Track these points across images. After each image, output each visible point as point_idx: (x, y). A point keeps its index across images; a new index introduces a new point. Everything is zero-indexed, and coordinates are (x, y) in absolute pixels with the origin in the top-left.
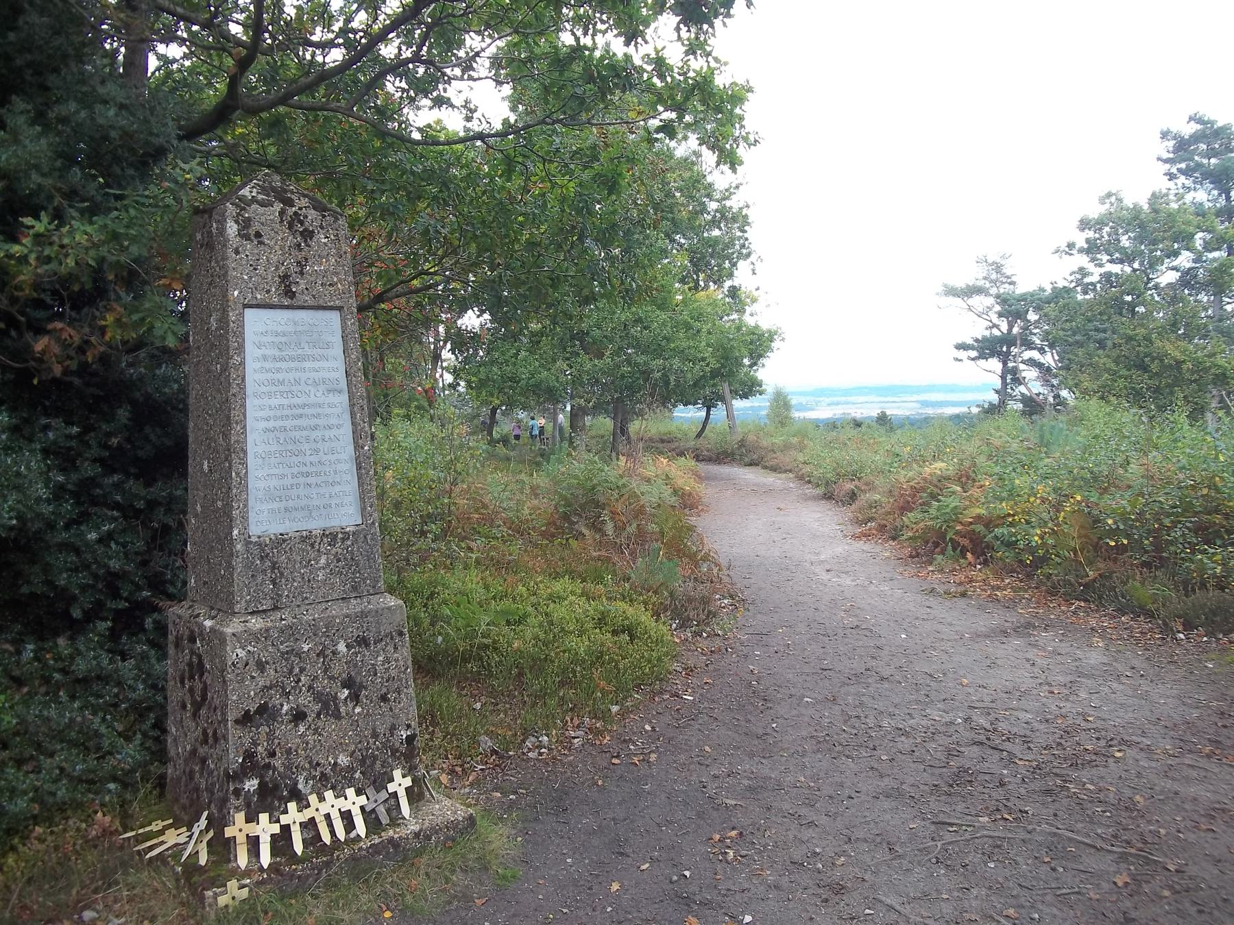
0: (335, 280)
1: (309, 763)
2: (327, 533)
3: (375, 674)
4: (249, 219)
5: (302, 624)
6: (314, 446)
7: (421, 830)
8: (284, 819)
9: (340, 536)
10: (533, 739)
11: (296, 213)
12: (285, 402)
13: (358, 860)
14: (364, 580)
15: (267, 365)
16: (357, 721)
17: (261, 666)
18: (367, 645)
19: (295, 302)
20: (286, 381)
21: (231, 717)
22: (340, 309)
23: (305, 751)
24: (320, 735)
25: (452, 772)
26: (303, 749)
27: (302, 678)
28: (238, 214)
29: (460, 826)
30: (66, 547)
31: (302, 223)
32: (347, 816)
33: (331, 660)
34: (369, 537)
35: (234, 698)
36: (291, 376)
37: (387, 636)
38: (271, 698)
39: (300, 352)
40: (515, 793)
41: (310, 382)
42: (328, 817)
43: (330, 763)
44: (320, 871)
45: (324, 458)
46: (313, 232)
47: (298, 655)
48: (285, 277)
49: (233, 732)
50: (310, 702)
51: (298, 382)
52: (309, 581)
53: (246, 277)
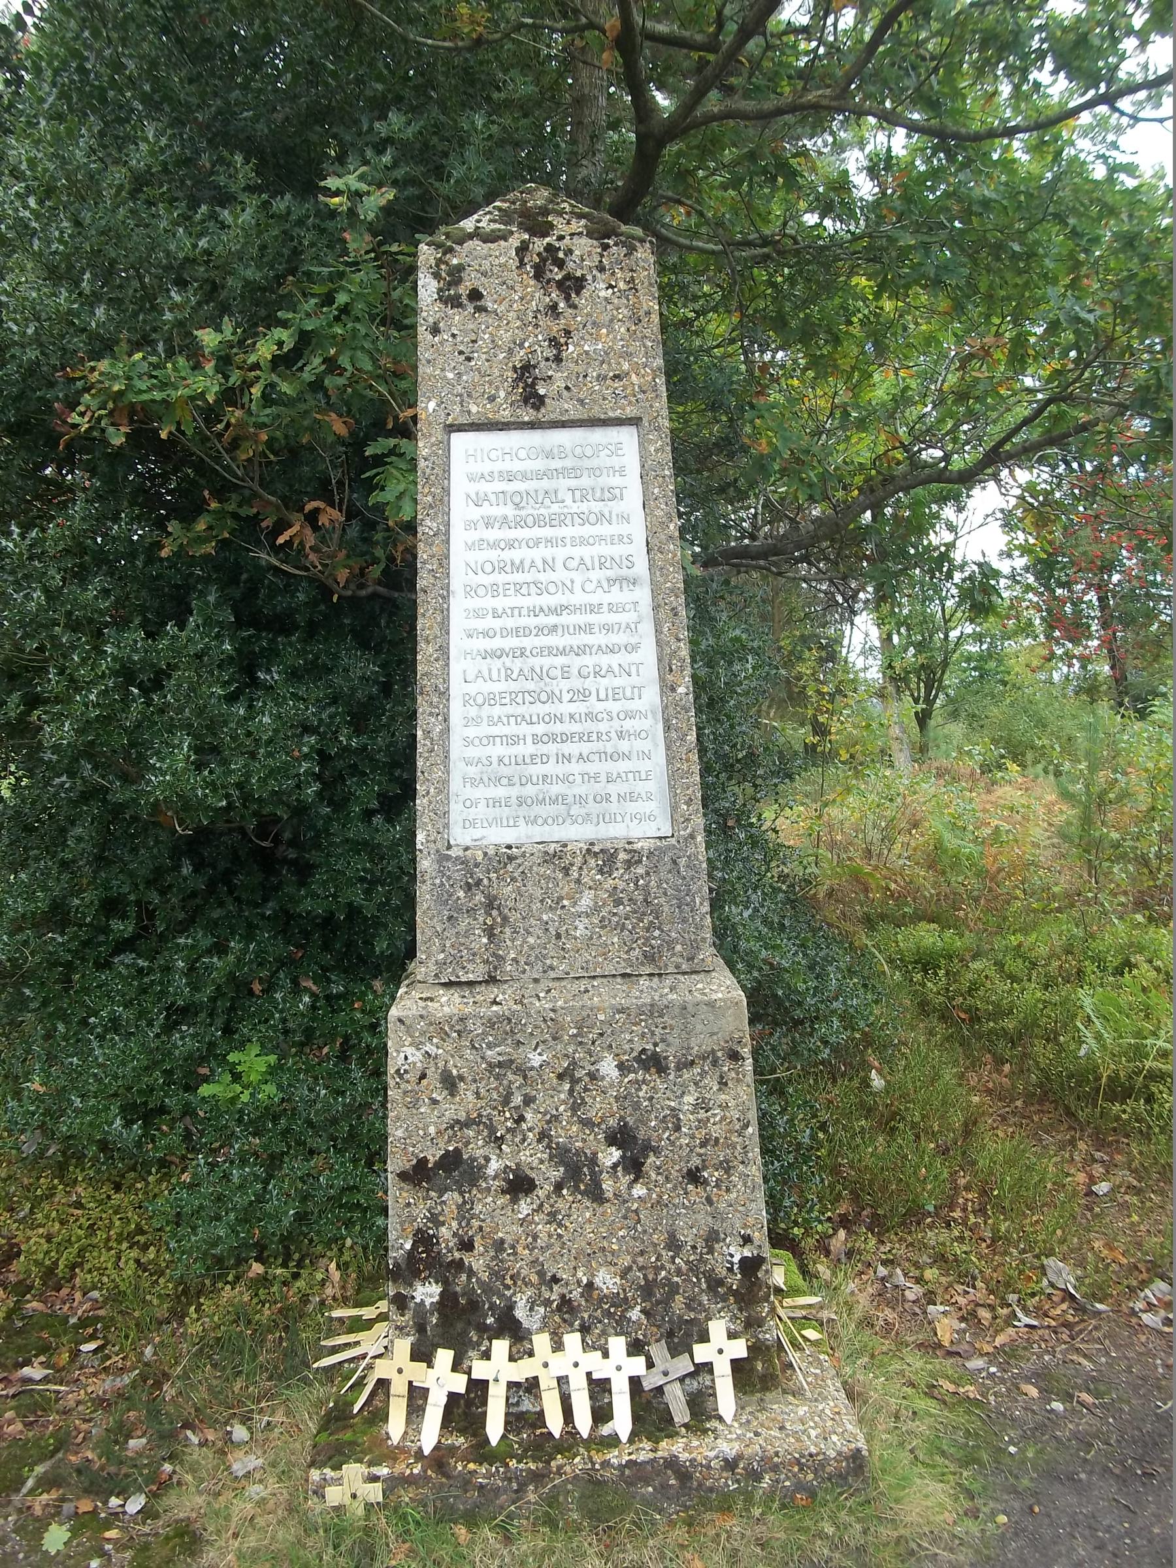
1: (538, 1273)
2: (596, 849)
3: (678, 1128)
4: (460, 268)
5: (529, 1015)
6: (577, 683)
7: (739, 1457)
8: (480, 1369)
9: (622, 856)
14: (670, 944)
15: (493, 534)
16: (636, 1211)
19: (544, 414)
20: (527, 565)
21: (396, 1163)
23: (531, 1250)
24: (560, 1225)
25: (969, 1317)
28: (439, 262)
29: (829, 1469)
30: (358, 847)
31: (561, 264)
32: (599, 1388)
33: (586, 1090)
34: (683, 862)
36: (537, 554)
37: (704, 1058)
38: (467, 1143)
39: (555, 508)
40: (1067, 1397)
41: (573, 564)
42: (562, 1381)
43: (579, 1282)
44: (521, 1490)
46: (583, 278)
47: (523, 1071)
48: (527, 367)
49: (397, 1195)
50: (542, 1162)
51: (549, 565)
52: (558, 936)
53: (450, 375)
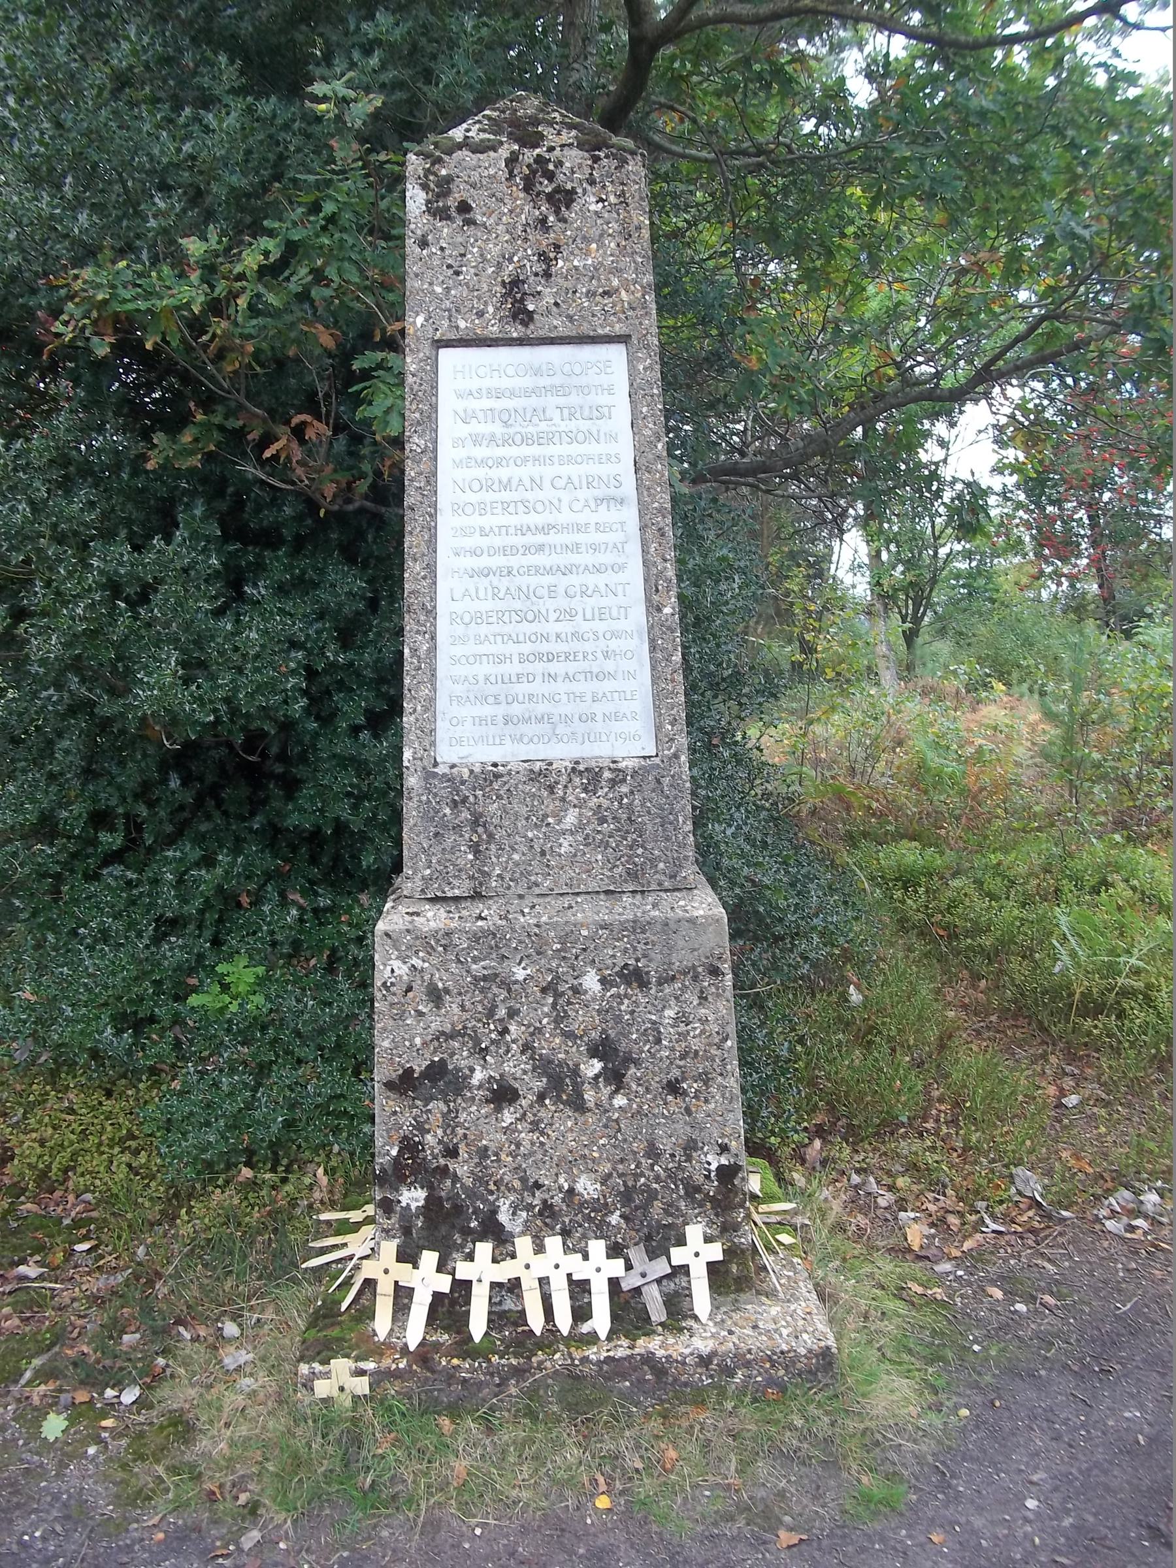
0: (616, 282)
1: (520, 1179)
2: (581, 767)
3: (658, 1041)
4: (449, 180)
5: (513, 930)
7: (713, 1354)
8: (464, 1270)
9: (607, 775)
10: (1127, 1194)
11: (539, 159)
12: (513, 520)
13: (577, 1378)
14: (653, 862)
15: (480, 452)
16: (617, 1121)
17: (436, 996)
18: (643, 984)
19: (532, 331)
20: (514, 483)
21: (382, 1072)
22: (623, 339)
23: (515, 1157)
24: (542, 1133)
25: (939, 1223)
26: (510, 1154)
27: (513, 1028)
28: (428, 172)
31: (551, 176)
32: (579, 1289)
33: (569, 1003)
34: (666, 781)
35: (386, 1044)
36: (524, 472)
37: (685, 974)
38: (452, 1054)
39: (543, 426)
41: (560, 483)
42: (544, 1282)
43: (560, 1188)
45: (586, 626)
46: (573, 191)
47: (507, 985)
49: (384, 1104)
51: (536, 483)
52: (543, 853)
53: (438, 290)
